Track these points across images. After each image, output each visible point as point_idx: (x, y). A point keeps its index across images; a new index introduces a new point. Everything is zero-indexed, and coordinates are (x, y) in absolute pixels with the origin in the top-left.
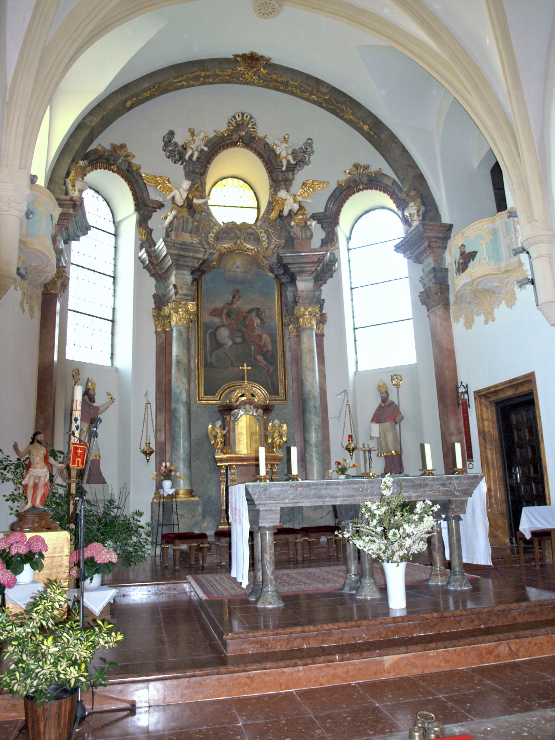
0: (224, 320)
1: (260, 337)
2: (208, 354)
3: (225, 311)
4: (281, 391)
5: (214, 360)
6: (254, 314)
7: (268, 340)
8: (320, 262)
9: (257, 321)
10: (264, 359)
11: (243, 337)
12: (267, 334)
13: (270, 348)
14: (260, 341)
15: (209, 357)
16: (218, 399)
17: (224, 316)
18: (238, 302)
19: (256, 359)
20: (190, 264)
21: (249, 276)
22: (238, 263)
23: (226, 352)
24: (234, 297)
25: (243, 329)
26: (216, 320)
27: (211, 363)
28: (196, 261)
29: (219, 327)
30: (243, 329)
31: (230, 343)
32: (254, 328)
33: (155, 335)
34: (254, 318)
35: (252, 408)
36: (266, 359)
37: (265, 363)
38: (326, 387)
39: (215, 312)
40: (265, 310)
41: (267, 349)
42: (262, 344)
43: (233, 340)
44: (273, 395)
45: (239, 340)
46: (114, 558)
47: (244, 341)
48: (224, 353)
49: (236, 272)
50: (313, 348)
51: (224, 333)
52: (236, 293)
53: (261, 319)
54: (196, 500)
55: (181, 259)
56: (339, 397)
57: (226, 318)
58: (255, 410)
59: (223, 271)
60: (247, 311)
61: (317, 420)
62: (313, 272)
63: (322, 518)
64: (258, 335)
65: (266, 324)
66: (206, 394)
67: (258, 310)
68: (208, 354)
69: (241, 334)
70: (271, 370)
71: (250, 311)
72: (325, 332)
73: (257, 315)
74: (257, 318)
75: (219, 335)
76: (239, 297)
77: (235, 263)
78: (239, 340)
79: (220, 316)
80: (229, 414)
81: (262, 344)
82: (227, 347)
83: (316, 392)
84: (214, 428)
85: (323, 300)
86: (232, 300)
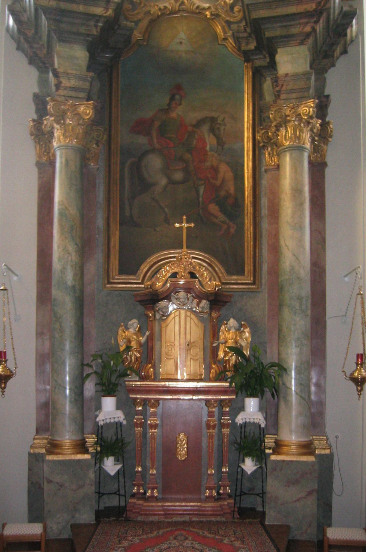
0: (155, 141)
1: (215, 170)
3: (157, 124)
4: (248, 267)
6: (205, 128)
7: (230, 175)
8: (321, 13)
9: (210, 141)
10: (221, 211)
12: (228, 164)
13: (232, 191)
14: (216, 178)
15: (127, 207)
17: (154, 134)
18: (180, 108)
20: (83, 30)
24: (172, 98)
26: (142, 140)
28: (92, 23)
29: (146, 153)
32: (206, 153)
33: (36, 170)
34: (206, 136)
35: (191, 299)
36: (223, 210)
37: (222, 217)
38: (325, 261)
41: (227, 192)
42: (218, 183)
43: (169, 178)
44: (233, 274)
45: (178, 176)
50: (303, 185)
53: (219, 139)
54: (86, 460)
55: (65, 19)
56: (346, 279)
58: (195, 301)
61: (302, 322)
62: (308, 35)
63: (298, 500)
64: (212, 167)
65: (226, 146)
66: (122, 272)
67: (213, 120)
68: (127, 202)
70: (232, 230)
71: (199, 124)
72: (329, 159)
73: (212, 130)
74: (211, 135)
78: (178, 176)
79: (148, 134)
80: (153, 309)
81: (218, 183)
83: (304, 268)
84: (130, 334)
85: (328, 97)
86: (169, 105)
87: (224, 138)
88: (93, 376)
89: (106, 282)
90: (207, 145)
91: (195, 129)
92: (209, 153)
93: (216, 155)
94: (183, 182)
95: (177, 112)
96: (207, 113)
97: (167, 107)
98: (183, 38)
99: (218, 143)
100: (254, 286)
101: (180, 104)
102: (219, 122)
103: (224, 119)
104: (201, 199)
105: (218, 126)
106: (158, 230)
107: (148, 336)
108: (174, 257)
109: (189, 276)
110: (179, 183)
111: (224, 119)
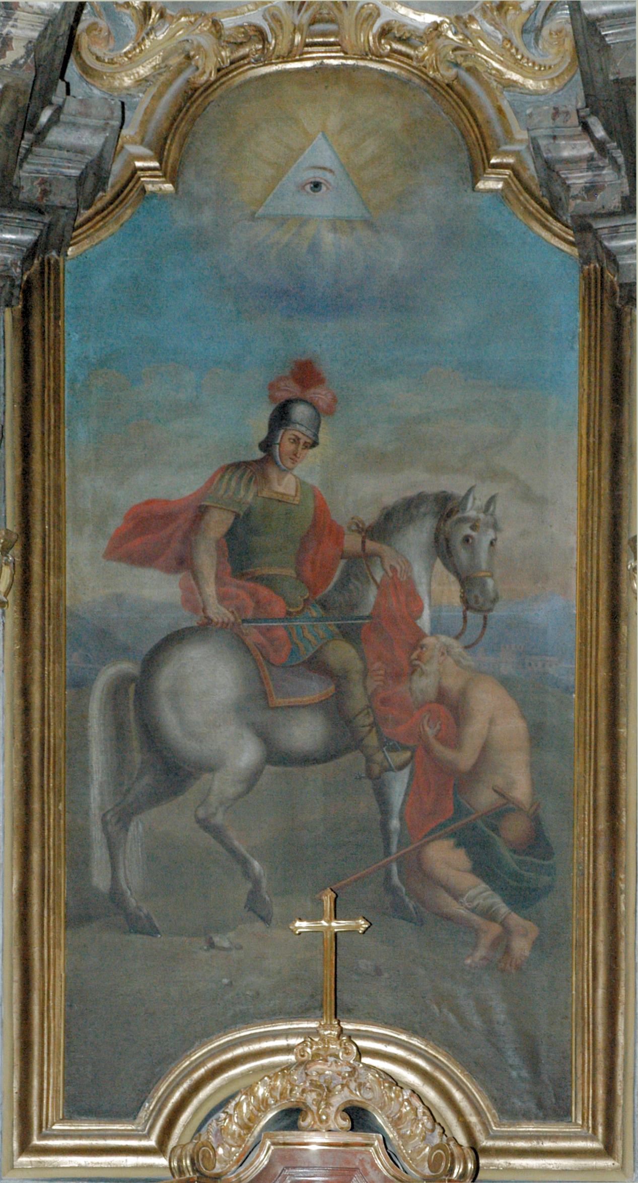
1: (453, 708)
2: (97, 833)
3: (218, 524)
5: (133, 877)
6: (415, 539)
9: (436, 592)
11: (335, 709)
12: (506, 682)
13: (522, 791)
14: (455, 743)
15: (99, 853)
16: (152, 1143)
19: (416, 867)
21: (395, 255)
22: (321, 154)
23: (219, 819)
24: (281, 416)
25: (342, 654)
26: (156, 589)
27: (116, 896)
29: (176, 638)
30: (342, 654)
31: (246, 754)
32: (417, 640)
36: (485, 867)
37: (479, 891)
39: (153, 536)
40: (498, 510)
43: (264, 736)
45: (306, 732)
46: (398, 7)
47: (345, 738)
48: (205, 824)
49: (303, 221)
51: (206, 687)
52: (292, 389)
53: (467, 581)
57: (219, 580)
59: (207, 217)
60: (369, 516)
64: (442, 695)
65: (499, 612)
66: (77, 1107)
67: (446, 507)
68: (97, 833)
69: (316, 689)
70: (521, 946)
71: (388, 524)
73: (442, 548)
75: (175, 694)
76: (318, 414)
77: (293, 155)
79: (184, 563)
81: (465, 758)
82: (223, 784)
86: (267, 445)
87: (490, 582)
88: (40, 226)
89: (16, 1145)
90: (421, 610)
91: (371, 545)
92: (429, 641)
93: (457, 647)
94: (328, 755)
95: (301, 475)
96: (421, 480)
97: (259, 454)
98: (328, 165)
99: (465, 601)
100: (607, 1163)
101: (315, 444)
102: (471, 513)
103: (492, 500)
104: (395, 823)
105: (467, 530)
106: (226, 944)
107: (523, 86)
108: (288, 1050)
109: (347, 1124)
110: (307, 760)
111: (492, 500)
